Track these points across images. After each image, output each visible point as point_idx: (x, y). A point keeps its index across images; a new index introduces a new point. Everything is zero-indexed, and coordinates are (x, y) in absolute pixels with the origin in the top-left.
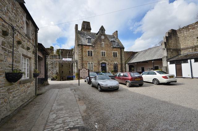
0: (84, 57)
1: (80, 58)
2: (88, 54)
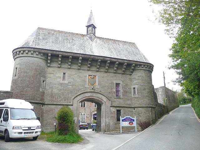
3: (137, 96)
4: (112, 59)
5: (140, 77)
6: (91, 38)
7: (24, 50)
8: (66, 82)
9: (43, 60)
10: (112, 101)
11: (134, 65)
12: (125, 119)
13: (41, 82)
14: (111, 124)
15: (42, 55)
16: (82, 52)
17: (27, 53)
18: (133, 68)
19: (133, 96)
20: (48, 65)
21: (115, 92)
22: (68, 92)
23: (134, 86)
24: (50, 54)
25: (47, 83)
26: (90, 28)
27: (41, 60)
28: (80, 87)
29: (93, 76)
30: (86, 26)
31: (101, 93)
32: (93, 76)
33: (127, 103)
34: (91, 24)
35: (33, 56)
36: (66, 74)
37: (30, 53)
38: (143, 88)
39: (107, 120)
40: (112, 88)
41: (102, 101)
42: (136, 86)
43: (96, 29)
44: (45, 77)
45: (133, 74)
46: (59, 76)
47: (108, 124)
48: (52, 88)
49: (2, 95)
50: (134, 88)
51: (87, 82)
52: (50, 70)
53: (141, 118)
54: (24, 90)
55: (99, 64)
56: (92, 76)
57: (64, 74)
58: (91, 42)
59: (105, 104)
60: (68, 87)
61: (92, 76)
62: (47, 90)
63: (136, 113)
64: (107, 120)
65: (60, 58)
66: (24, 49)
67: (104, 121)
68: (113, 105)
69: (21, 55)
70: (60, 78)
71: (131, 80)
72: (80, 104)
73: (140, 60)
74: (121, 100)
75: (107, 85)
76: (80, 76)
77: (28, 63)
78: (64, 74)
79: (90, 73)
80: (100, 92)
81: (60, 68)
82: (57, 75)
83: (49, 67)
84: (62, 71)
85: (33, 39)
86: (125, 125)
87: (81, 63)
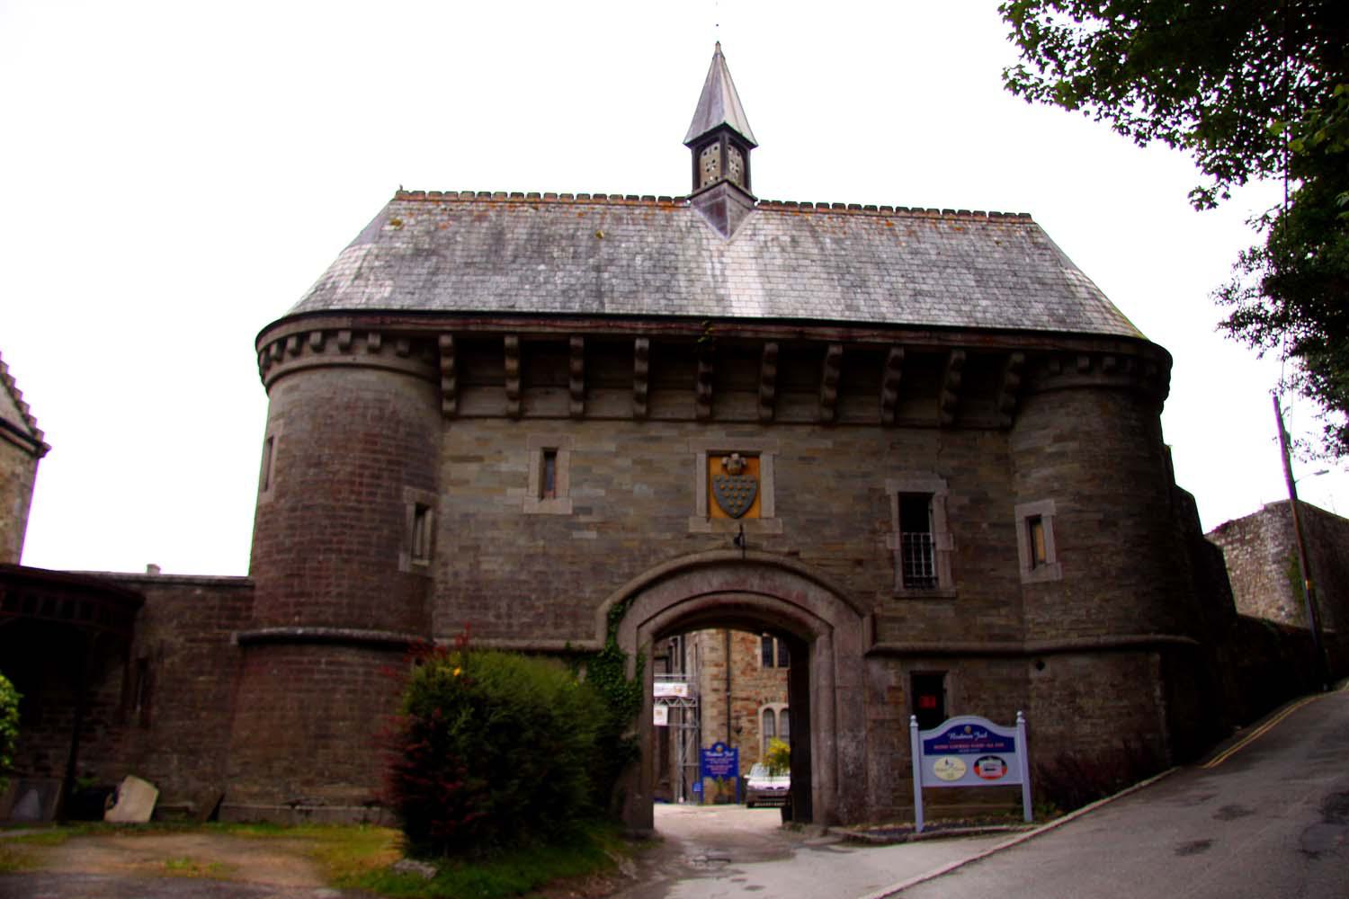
0: (736, 672)
1: (716, 684)
2: (760, 659)
3: (1053, 573)
4: (856, 333)
5: (1074, 439)
6: (717, 213)
7: (282, 335)
8: (561, 505)
9: (413, 379)
10: (874, 619)
11: (1018, 358)
12: (944, 739)
13: (403, 515)
14: (874, 770)
15: (402, 347)
16: (649, 304)
17: (319, 349)
18: (1013, 379)
19: (1026, 576)
20: (449, 406)
21: (898, 558)
22: (575, 568)
23: (1022, 511)
24: (446, 341)
25: (442, 519)
26: (713, 153)
27: (396, 382)
28: (652, 535)
29: (735, 456)
30: (689, 145)
31: (798, 566)
32: (735, 456)
33: (989, 626)
34: (714, 124)
35: (349, 359)
36: (563, 458)
37: (332, 347)
38: (1101, 516)
39: (847, 746)
40: (874, 532)
41: (810, 621)
42: (1048, 507)
43: (753, 153)
44: (431, 483)
45: (1022, 423)
46: (515, 475)
47: (855, 776)
48: (478, 547)
49: (203, 599)
50: (1034, 521)
51: (701, 502)
52: (460, 437)
53: (1087, 729)
54: (307, 566)
55: (896, 375)
56: (729, 454)
57: (550, 455)
58: (720, 235)
59: (831, 636)
60: (576, 535)
61: (729, 454)
62: (445, 565)
63: (1051, 695)
64: (847, 746)
65: (513, 353)
66: (303, 326)
67: (826, 752)
68: (881, 645)
69: (291, 363)
70: (522, 481)
71: (1005, 462)
72: (758, 651)
73: (1062, 321)
74: (946, 612)
75: (836, 507)
76: (650, 462)
77: (327, 407)
78: (550, 455)
79: (716, 437)
80: (788, 562)
81: (524, 424)
82: (504, 467)
83: (454, 417)
84: (536, 436)
85: (357, 265)
86: (943, 775)
87: (584, 376)
